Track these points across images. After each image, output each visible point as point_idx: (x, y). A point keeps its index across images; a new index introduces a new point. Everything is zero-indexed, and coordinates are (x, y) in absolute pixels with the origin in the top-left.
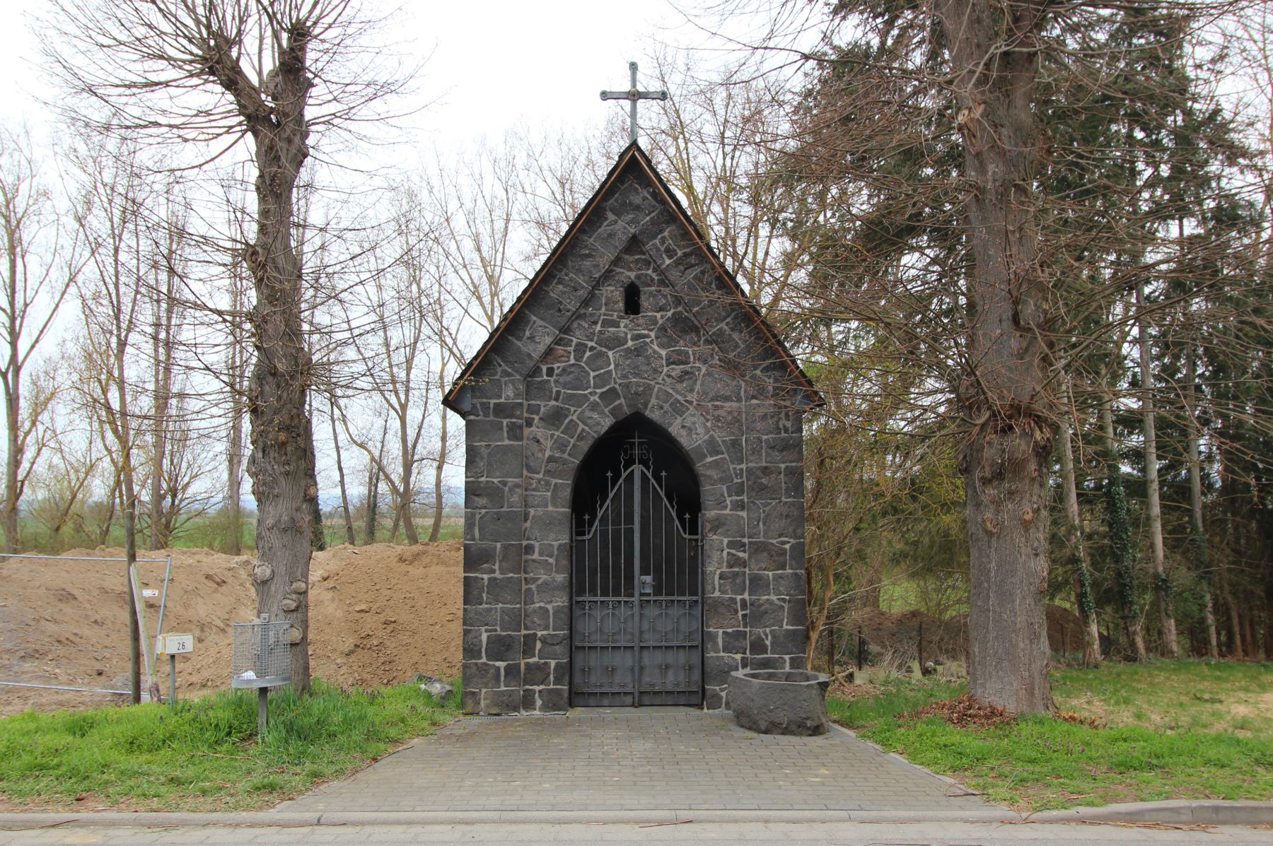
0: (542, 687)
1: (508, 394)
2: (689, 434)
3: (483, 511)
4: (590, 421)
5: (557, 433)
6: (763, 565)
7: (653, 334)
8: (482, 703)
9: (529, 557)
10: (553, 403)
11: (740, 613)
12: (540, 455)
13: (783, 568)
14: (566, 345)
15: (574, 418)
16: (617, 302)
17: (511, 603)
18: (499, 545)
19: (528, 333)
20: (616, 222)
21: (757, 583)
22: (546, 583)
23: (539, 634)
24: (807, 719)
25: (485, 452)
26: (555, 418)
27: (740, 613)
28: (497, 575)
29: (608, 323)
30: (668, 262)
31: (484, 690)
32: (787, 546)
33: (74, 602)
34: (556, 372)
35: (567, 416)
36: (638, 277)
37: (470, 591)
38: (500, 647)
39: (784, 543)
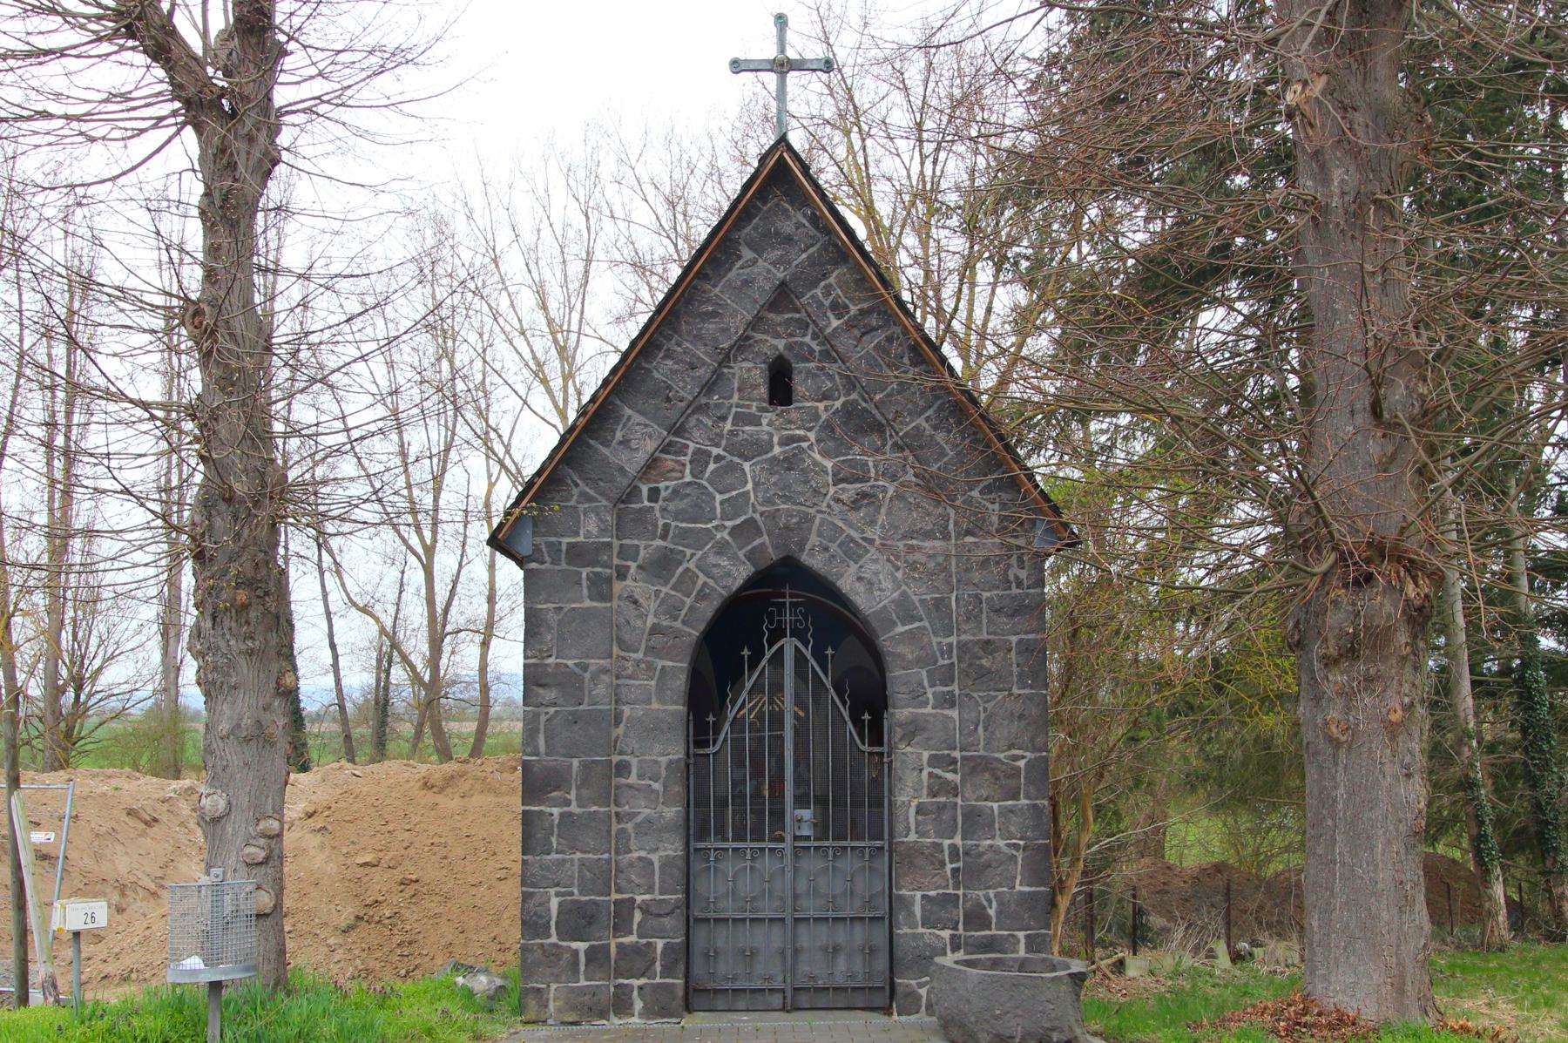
0: (643, 981)
1: (590, 528)
2: (870, 590)
3: (552, 710)
4: (715, 571)
5: (665, 590)
8: (551, 1004)
9: (623, 781)
10: (658, 542)
11: (949, 867)
12: (639, 623)
13: (1015, 797)
14: (677, 453)
15: (691, 565)
18: (575, 762)
19: (619, 435)
20: (755, 262)
21: (975, 821)
23: (639, 899)
24: (1052, 1029)
25: (553, 618)
26: (661, 566)
27: (949, 867)
28: (574, 808)
29: (740, 419)
30: (835, 323)
31: (554, 986)
32: (1022, 763)
34: (663, 494)
35: (680, 563)
36: (789, 347)
38: (579, 920)
39: (1016, 758)
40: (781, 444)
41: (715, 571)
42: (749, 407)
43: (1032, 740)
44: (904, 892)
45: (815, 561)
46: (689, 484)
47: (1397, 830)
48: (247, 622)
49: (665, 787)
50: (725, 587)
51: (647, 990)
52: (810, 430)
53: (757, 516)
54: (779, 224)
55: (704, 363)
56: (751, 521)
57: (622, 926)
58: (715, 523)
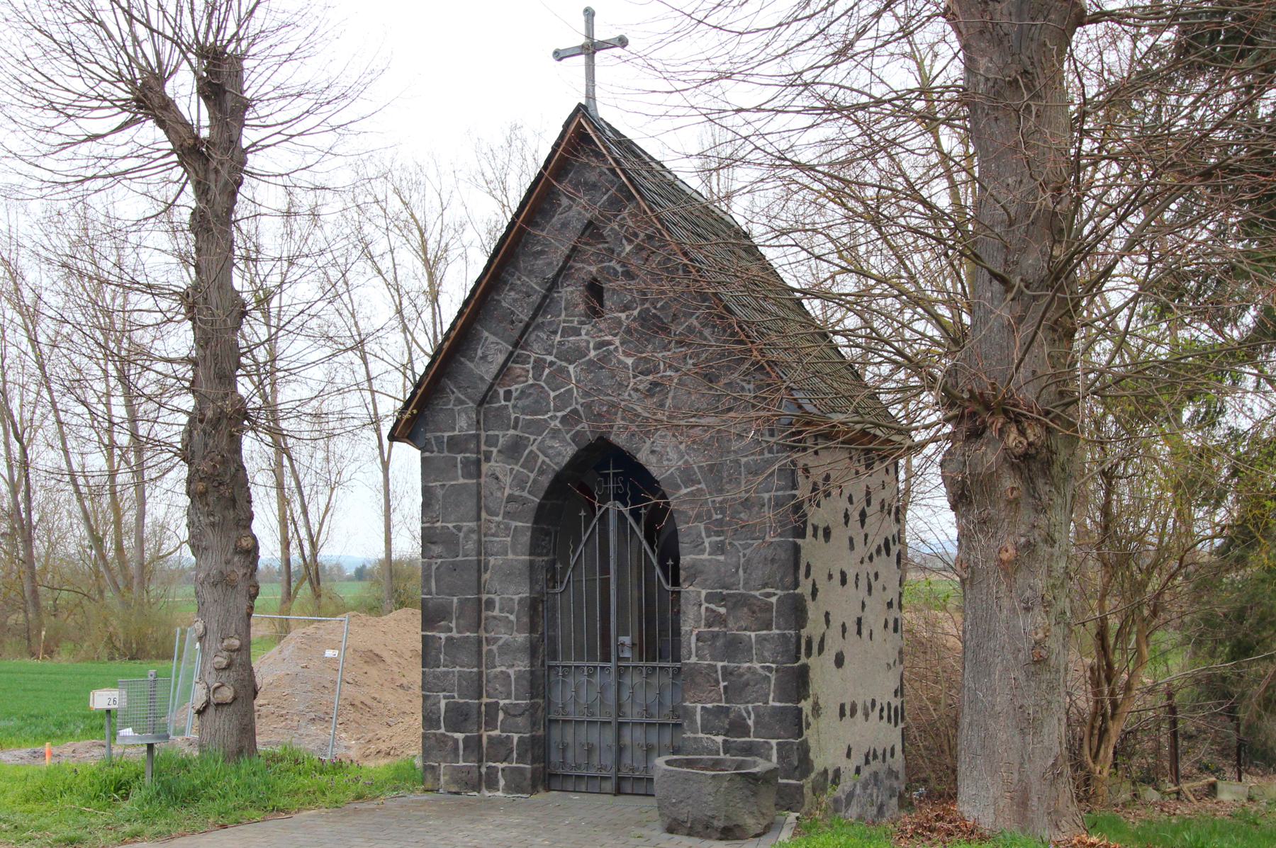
0: (505, 764)
1: (463, 424)
2: (660, 461)
3: (439, 561)
4: (550, 451)
5: (516, 468)
6: (743, 624)
7: (617, 341)
8: (442, 778)
9: (490, 613)
10: (512, 432)
11: (722, 684)
12: (499, 494)
13: (768, 627)
14: (523, 363)
15: (534, 448)
16: (576, 305)
17: (468, 666)
18: (455, 599)
19: (480, 353)
20: (570, 207)
21: (734, 648)
22: (506, 644)
23: (502, 702)
24: (713, 817)
25: (440, 493)
26: (514, 450)
27: (722, 684)
28: (455, 634)
29: (569, 332)
30: (628, 248)
31: (443, 765)
32: (774, 600)
33: (381, 665)
34: (515, 395)
35: (526, 447)
36: (601, 270)
37: (428, 654)
38: (458, 717)
39: (769, 595)
40: (595, 349)
41: (550, 451)
42: (572, 322)
43: (781, 580)
44: (687, 704)
45: (619, 439)
46: (532, 385)
47: (1016, 658)
48: (207, 504)
49: (517, 618)
50: (557, 464)
51: (507, 772)
52: (615, 335)
53: (579, 407)
54: (587, 175)
55: (536, 291)
56: (575, 411)
57: (491, 724)
58: (550, 414)
